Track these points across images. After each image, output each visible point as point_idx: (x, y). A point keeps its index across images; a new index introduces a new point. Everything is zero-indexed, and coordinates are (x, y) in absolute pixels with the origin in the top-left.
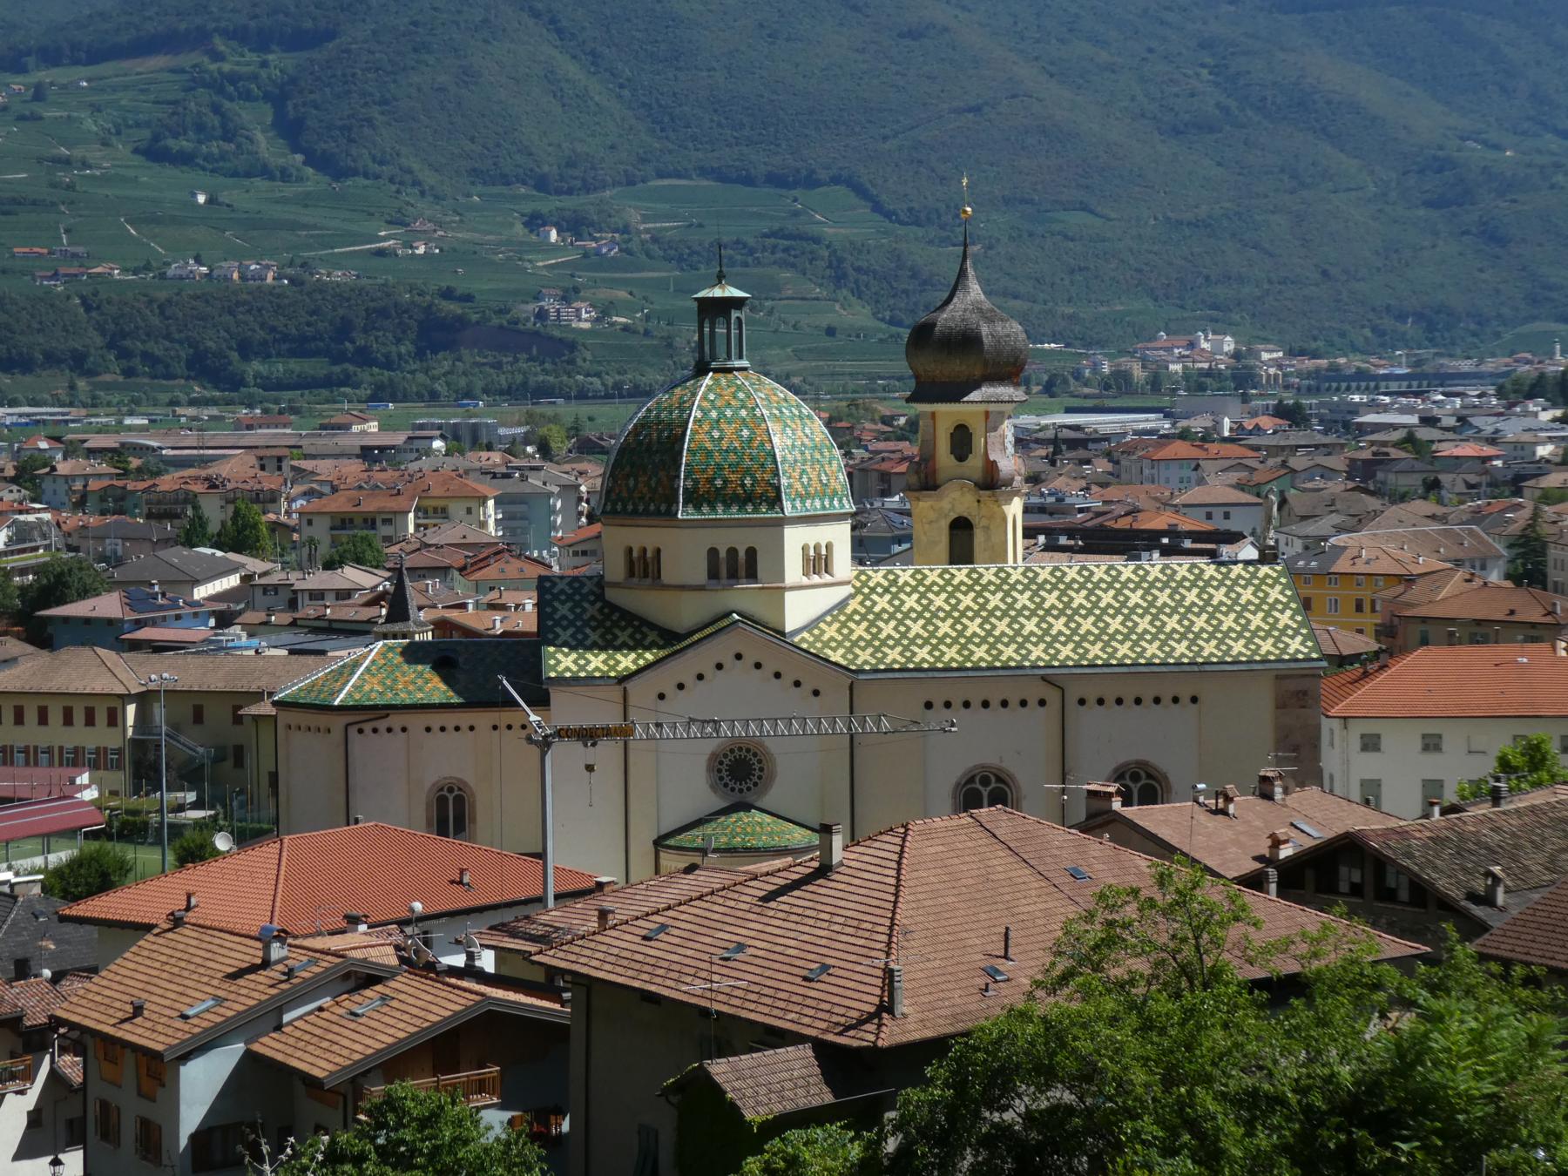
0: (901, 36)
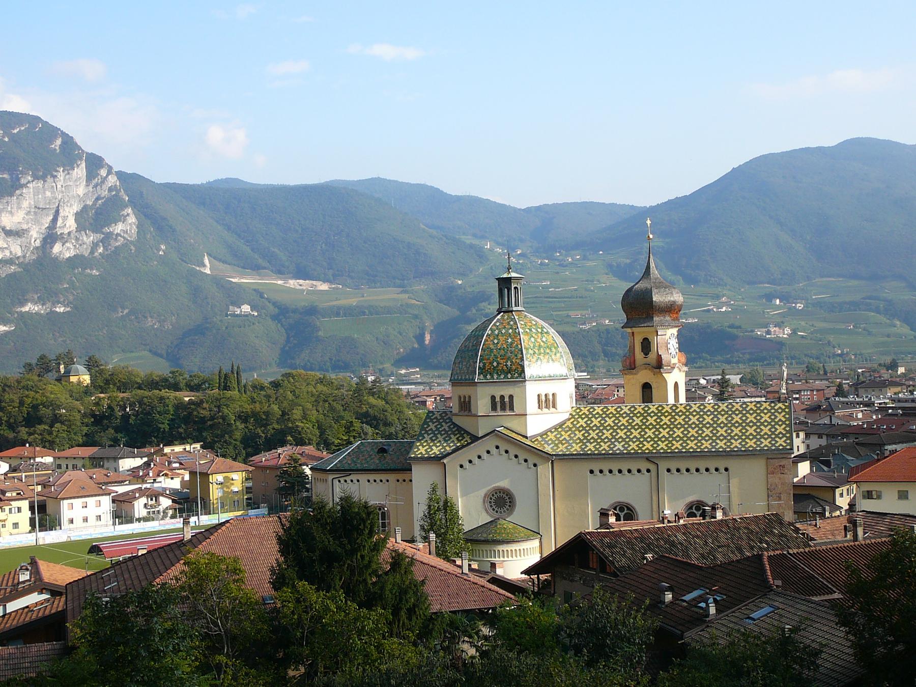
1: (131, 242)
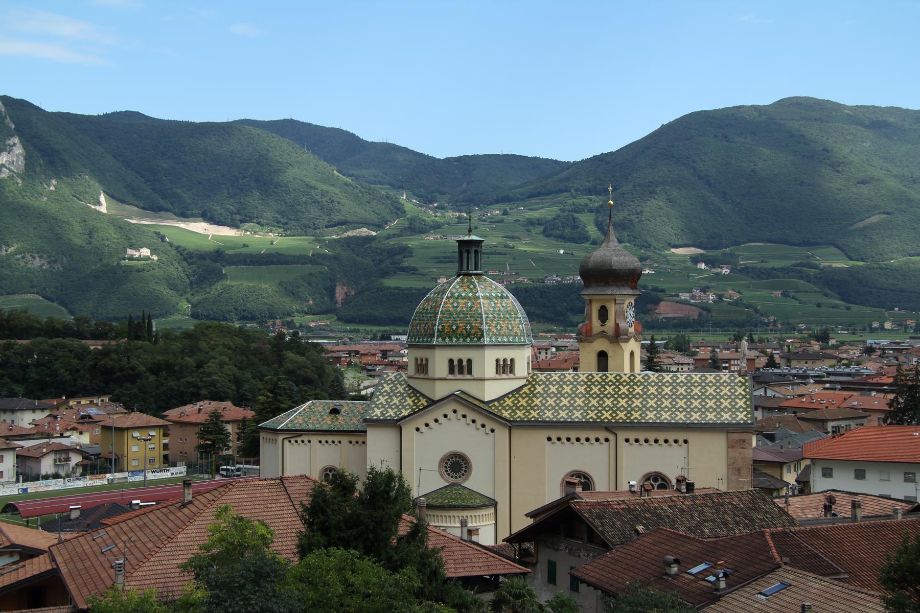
0: (858, 183)
1: (18, 175)
